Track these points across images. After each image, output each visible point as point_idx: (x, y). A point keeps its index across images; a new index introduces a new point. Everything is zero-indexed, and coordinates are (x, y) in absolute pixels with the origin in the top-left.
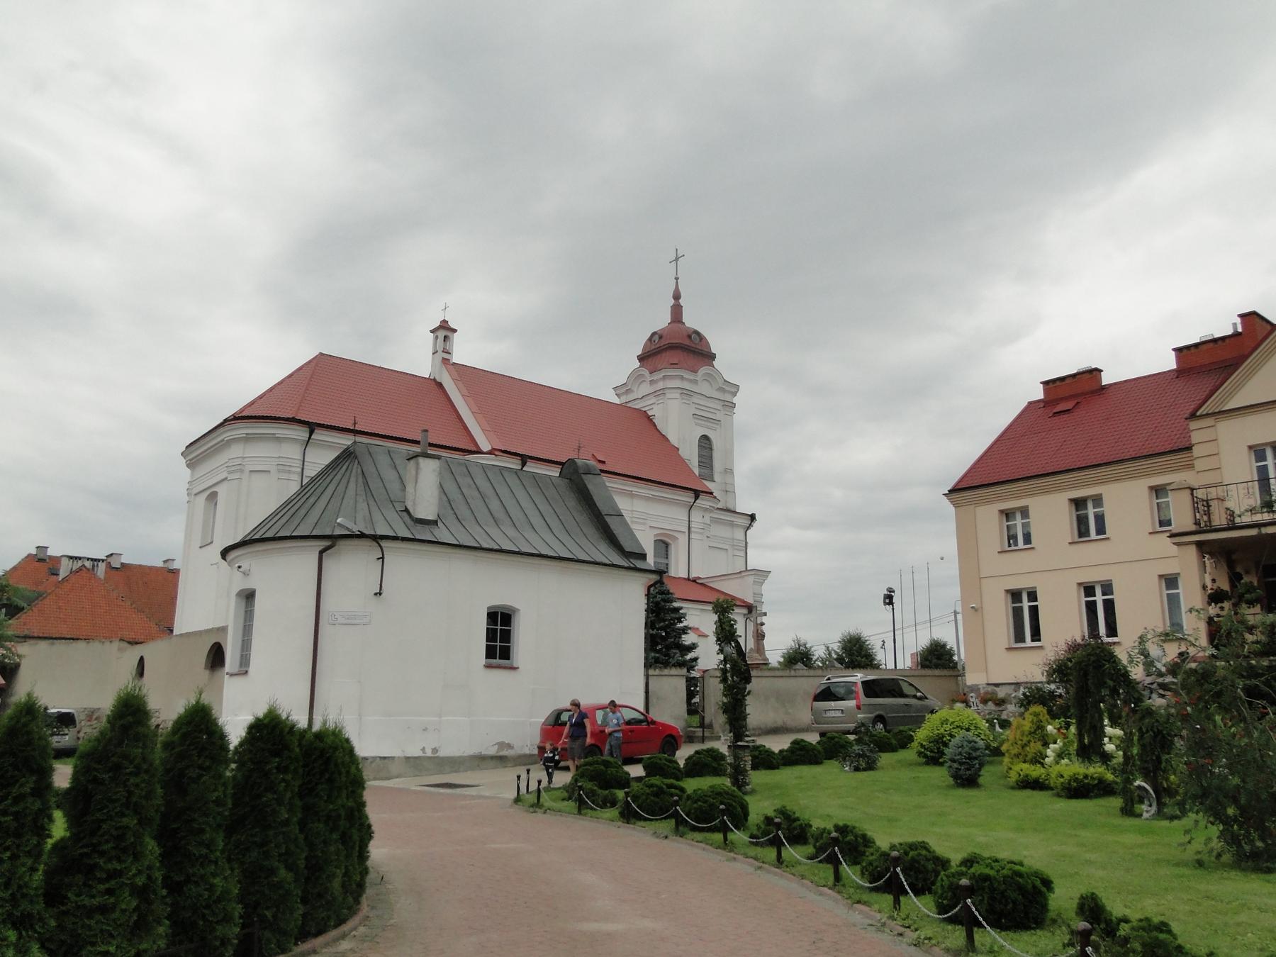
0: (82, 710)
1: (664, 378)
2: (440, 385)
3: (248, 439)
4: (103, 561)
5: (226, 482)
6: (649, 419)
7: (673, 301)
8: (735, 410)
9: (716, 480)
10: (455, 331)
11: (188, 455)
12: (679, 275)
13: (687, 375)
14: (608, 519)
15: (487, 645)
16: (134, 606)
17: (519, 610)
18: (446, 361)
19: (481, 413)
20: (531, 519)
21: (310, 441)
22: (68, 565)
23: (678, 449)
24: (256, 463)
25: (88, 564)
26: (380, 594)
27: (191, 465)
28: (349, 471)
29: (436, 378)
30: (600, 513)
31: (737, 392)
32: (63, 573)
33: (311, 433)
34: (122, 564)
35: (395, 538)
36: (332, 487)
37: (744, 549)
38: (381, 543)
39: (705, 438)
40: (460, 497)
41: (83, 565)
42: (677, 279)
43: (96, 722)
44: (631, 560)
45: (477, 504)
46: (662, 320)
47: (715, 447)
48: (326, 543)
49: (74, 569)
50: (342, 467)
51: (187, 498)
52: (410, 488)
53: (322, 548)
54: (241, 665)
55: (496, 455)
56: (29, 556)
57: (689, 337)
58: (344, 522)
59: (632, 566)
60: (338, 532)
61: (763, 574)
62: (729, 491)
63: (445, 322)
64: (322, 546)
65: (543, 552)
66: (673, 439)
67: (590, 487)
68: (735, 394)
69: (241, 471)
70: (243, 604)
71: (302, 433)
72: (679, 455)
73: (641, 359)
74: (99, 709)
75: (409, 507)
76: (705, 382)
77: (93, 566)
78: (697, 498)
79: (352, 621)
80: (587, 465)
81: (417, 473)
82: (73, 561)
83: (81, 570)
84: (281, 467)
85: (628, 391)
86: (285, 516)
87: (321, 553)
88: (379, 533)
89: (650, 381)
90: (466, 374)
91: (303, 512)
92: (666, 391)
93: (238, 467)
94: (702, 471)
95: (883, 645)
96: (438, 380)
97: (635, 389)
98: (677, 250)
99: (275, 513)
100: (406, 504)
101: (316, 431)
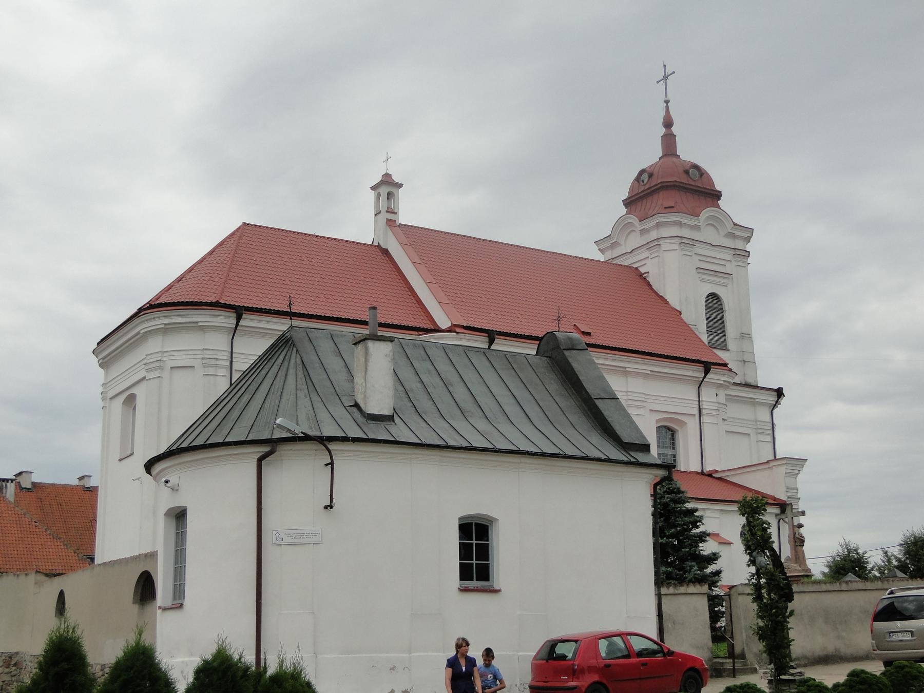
1: (658, 225)
2: (386, 252)
3: (167, 330)
5: (145, 382)
7: (663, 130)
10: (400, 186)
12: (669, 97)
13: (687, 220)
14: (599, 403)
17: (496, 520)
18: (391, 223)
21: (238, 328)
23: (680, 313)
26: (331, 507)
28: (286, 363)
34: (34, 484)
35: (345, 439)
37: (771, 432)
40: (419, 385)
42: (667, 102)
43: (14, 668)
47: (726, 307)
48: (265, 449)
52: (359, 379)
53: (259, 455)
55: (457, 333)
57: (687, 172)
59: (633, 460)
60: (278, 435)
62: (747, 361)
63: (387, 176)
64: (262, 452)
66: (674, 300)
68: (748, 240)
69: (161, 368)
71: (227, 320)
72: (682, 319)
73: (628, 203)
74: (17, 653)
78: (707, 372)
81: (366, 361)
84: (206, 361)
85: (614, 245)
87: (260, 461)
89: (640, 230)
91: (236, 413)
93: (157, 364)
94: (712, 337)
96: (383, 246)
97: (622, 242)
98: (665, 66)
99: (204, 416)
101: (244, 316)
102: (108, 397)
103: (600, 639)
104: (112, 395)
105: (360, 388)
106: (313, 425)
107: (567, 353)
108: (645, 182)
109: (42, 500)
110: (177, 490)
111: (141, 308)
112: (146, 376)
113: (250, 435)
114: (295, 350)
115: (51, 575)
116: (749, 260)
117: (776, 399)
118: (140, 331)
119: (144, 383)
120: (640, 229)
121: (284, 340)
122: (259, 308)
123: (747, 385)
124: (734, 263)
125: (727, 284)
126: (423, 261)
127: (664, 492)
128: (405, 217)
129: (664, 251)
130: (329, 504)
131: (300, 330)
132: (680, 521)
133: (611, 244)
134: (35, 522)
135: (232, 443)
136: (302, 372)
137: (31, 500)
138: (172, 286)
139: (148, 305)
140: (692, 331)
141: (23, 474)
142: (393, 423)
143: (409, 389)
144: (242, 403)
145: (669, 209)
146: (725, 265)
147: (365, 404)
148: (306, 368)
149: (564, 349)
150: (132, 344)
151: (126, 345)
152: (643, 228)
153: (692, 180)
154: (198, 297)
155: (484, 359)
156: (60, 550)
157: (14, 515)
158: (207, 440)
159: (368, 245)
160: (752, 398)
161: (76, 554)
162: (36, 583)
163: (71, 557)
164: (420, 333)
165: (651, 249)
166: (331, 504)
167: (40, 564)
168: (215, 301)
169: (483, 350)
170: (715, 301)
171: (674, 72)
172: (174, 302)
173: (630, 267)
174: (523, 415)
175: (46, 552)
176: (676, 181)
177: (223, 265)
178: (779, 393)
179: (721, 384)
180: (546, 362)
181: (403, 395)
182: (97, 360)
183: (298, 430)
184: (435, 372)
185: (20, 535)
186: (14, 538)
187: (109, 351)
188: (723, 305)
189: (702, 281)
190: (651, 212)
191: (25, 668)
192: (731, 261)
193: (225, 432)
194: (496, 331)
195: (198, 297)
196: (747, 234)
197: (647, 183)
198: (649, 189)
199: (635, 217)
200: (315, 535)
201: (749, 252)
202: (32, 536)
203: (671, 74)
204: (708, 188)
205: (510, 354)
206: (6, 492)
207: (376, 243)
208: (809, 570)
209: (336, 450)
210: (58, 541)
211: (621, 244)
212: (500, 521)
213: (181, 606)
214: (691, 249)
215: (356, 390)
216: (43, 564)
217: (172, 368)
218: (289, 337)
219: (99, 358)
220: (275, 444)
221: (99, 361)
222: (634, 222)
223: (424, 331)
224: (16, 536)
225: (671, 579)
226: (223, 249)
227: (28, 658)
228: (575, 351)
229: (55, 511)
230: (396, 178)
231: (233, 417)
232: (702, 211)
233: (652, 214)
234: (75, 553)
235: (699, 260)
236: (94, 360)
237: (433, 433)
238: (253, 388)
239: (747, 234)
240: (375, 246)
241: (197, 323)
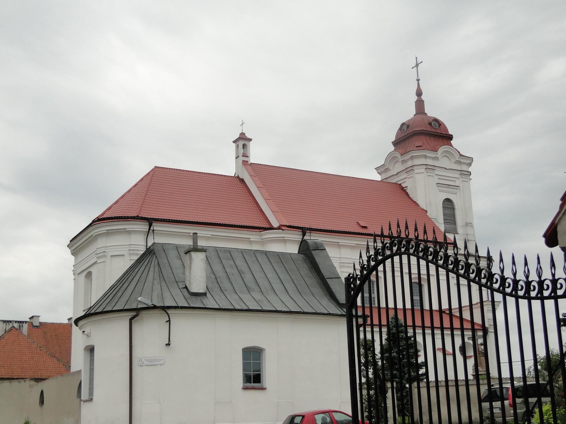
1: (412, 158)
2: (242, 181)
3: (108, 233)
4: (26, 322)
5: (96, 265)
6: (403, 190)
11: (71, 247)
12: (419, 77)
14: (329, 281)
16: (48, 353)
17: (265, 349)
18: (245, 163)
22: (3, 326)
23: (426, 212)
24: (115, 250)
25: (16, 325)
26: (169, 345)
27: (74, 253)
28: (149, 264)
30: (324, 277)
33: (150, 225)
34: (40, 323)
38: (167, 312)
39: (448, 202)
40: (224, 274)
41: (13, 327)
42: (418, 80)
45: (236, 278)
46: (409, 113)
47: (456, 207)
48: (133, 314)
49: (7, 330)
50: (147, 259)
51: (73, 277)
52: (187, 273)
53: (130, 317)
54: (90, 396)
55: (283, 230)
58: (144, 300)
60: (140, 306)
63: (242, 134)
64: (131, 315)
65: (279, 309)
66: (422, 205)
68: (470, 164)
69: (105, 256)
70: (89, 354)
71: (144, 227)
72: (427, 216)
73: (395, 143)
75: (188, 285)
77: (20, 326)
79: (152, 363)
81: (191, 263)
82: (6, 324)
83: (12, 330)
85: (387, 170)
86: (111, 295)
87: (131, 320)
88: (167, 304)
89: (401, 161)
91: (120, 293)
92: (415, 168)
93: (103, 254)
94: (447, 226)
96: (241, 177)
98: (416, 58)
99: (105, 295)
101: (153, 224)
102: (77, 273)
103: (315, 415)
104: (79, 272)
105: (188, 278)
106: (160, 300)
108: (405, 130)
109: (46, 333)
110: (90, 336)
111: (94, 220)
112: (97, 261)
113: (126, 306)
114: (155, 256)
115: (38, 380)
116: (471, 177)
119: (96, 266)
120: (401, 160)
121: (150, 251)
122: (163, 219)
124: (461, 180)
125: (457, 192)
126: (264, 186)
127: (393, 327)
128: (253, 159)
130: (168, 343)
131: (159, 245)
132: (402, 343)
133: (385, 169)
134: (40, 347)
136: (158, 269)
137: (39, 333)
138: (112, 207)
139: (97, 219)
140: (433, 223)
141: (34, 317)
142: (206, 297)
143: (218, 277)
144: (125, 286)
146: (455, 181)
147: (190, 287)
148: (160, 268)
149: (312, 250)
150: (81, 247)
151: (86, 242)
153: (434, 128)
154: (129, 214)
155: (265, 257)
156: (55, 364)
157: (27, 343)
158: (104, 309)
159: (231, 177)
161: (64, 367)
162: (30, 386)
163: (61, 368)
164: (261, 230)
165: (408, 172)
167: (43, 373)
169: (265, 252)
170: (449, 203)
172: (112, 217)
173: (396, 184)
174: (284, 289)
175: (47, 365)
177: (142, 193)
180: (302, 257)
181: (214, 280)
183: (150, 304)
184: (235, 266)
185: (31, 355)
186: (27, 357)
187: (83, 241)
188: (454, 206)
189: (440, 191)
190: (408, 149)
192: (458, 178)
194: (307, 228)
195: (129, 214)
196: (469, 161)
197: (406, 130)
198: (407, 135)
199: (398, 153)
200: (161, 360)
201: (470, 172)
202: (38, 356)
203: (420, 63)
204: (444, 133)
205: (281, 253)
206: (22, 329)
207: (236, 176)
210: (54, 358)
211: (391, 169)
213: (92, 399)
214: (433, 172)
215: (186, 279)
216: (45, 373)
217: (111, 256)
218: (152, 249)
219: (72, 250)
220: (138, 311)
222: (398, 156)
223: (263, 229)
224: (29, 356)
225: (396, 378)
226: (142, 183)
228: (318, 251)
229: (54, 340)
230: (248, 135)
231: (118, 296)
232: (439, 148)
233: (409, 151)
234: (64, 365)
235: (438, 178)
236: (69, 251)
237: (228, 302)
238: (130, 279)
239: (469, 161)
240: (236, 177)
241: (126, 229)
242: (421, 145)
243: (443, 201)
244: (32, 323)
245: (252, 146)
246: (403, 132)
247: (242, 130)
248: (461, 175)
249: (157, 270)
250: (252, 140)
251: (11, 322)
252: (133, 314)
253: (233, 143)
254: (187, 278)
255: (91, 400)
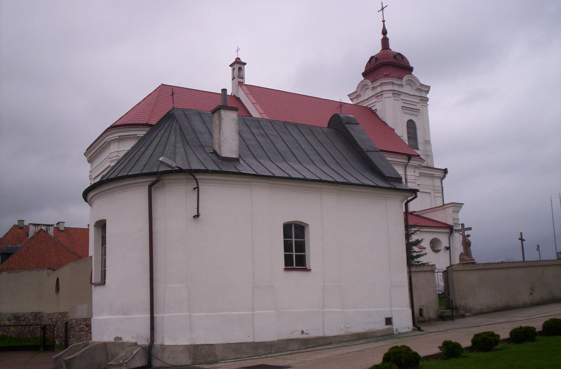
0: (31, 313)
1: (382, 84)
6: (373, 113)
8: (428, 103)
9: (419, 149)
10: (245, 64)
12: (384, 19)
14: (369, 154)
15: (285, 255)
19: (266, 113)
20: (311, 157)
25: (44, 228)
27: (90, 161)
28: (169, 128)
29: (236, 95)
31: (428, 91)
32: (31, 234)
34: (65, 227)
35: (206, 171)
36: (158, 139)
37: (441, 192)
41: (41, 229)
42: (384, 21)
43: (38, 321)
44: (391, 183)
46: (376, 49)
47: (418, 127)
48: (154, 179)
49: (36, 232)
52: (216, 136)
53: (150, 183)
56: (15, 226)
59: (393, 187)
60: (163, 169)
61: (458, 206)
62: (429, 155)
66: (390, 123)
67: (352, 132)
68: (427, 92)
73: (364, 75)
74: (40, 313)
76: (408, 85)
77: (47, 229)
80: (348, 117)
81: (220, 123)
82: (35, 227)
83: (40, 231)
85: (358, 96)
87: (150, 187)
89: (372, 88)
90: (254, 90)
95: (538, 248)
97: (362, 94)
98: (382, 3)
100: (214, 147)
105: (217, 141)
107: (347, 126)
114: (175, 121)
117: (443, 175)
118: (106, 141)
120: (372, 87)
123: (428, 167)
124: (421, 104)
128: (248, 81)
129: (385, 98)
135: (132, 176)
141: (60, 223)
145: (387, 76)
147: (220, 150)
149: (345, 123)
152: (373, 86)
160: (431, 174)
166: (197, 214)
168: (145, 123)
171: (387, 6)
176: (390, 61)
178: (445, 171)
179: (417, 166)
182: (87, 158)
189: (405, 113)
191: (44, 321)
193: (128, 170)
197: (375, 62)
198: (375, 66)
207: (233, 95)
208: (474, 260)
209: (201, 179)
212: (310, 225)
219: (88, 157)
221: (87, 159)
227: (45, 315)
230: (243, 60)
235: (403, 103)
236: (85, 159)
239: (427, 89)
240: (232, 96)
242: (389, 74)
243: (407, 122)
244: (58, 228)
245: (247, 69)
246: (372, 64)
247: (238, 55)
248: (422, 100)
249: (178, 133)
250: (246, 64)
251: (39, 225)
252: (154, 179)
253: (230, 66)
254: (216, 141)
255: (103, 283)
